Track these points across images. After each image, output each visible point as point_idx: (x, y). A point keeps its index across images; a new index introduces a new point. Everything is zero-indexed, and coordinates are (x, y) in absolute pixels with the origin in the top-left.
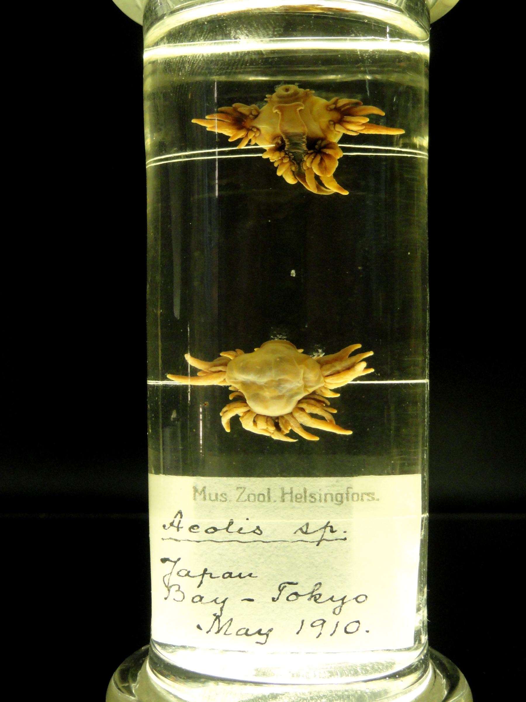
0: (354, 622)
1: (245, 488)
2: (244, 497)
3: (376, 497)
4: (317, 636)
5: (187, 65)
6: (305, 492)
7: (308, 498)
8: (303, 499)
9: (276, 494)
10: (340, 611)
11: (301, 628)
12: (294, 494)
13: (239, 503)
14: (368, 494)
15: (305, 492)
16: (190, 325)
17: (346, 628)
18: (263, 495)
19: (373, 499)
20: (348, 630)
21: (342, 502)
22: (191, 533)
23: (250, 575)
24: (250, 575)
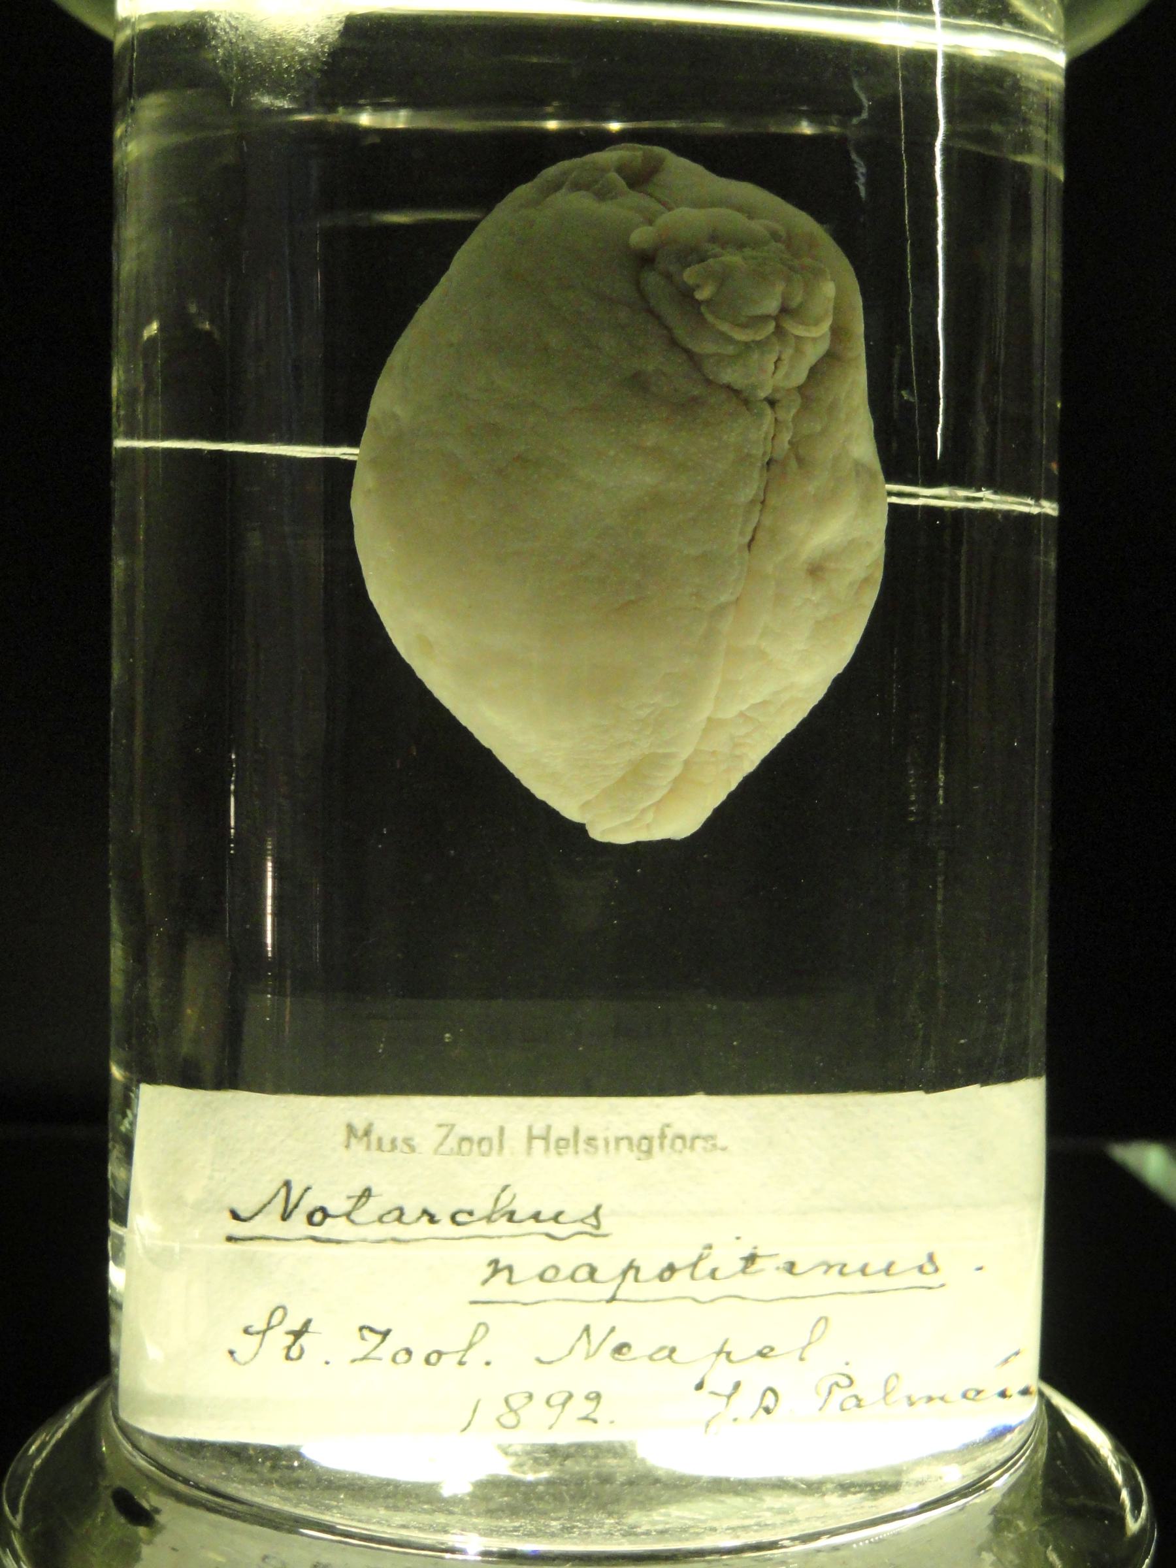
0: (679, 1363)
1: (453, 1126)
2: (452, 1142)
3: (720, 1142)
4: (480, 1402)
5: (950, 85)
6: (576, 1132)
7: (582, 1146)
8: (571, 1150)
9: (427, 1138)
10: (887, 1382)
11: (556, 1421)
12: (553, 1140)
13: (438, 1158)
14: (706, 1138)
15: (576, 1132)
16: (236, 777)
17: (842, 1404)
18: (490, 1139)
19: (714, 1146)
20: (844, 1407)
21: (649, 1152)
22: (594, 1283)
23: (942, 1399)
24: (942, 1399)
